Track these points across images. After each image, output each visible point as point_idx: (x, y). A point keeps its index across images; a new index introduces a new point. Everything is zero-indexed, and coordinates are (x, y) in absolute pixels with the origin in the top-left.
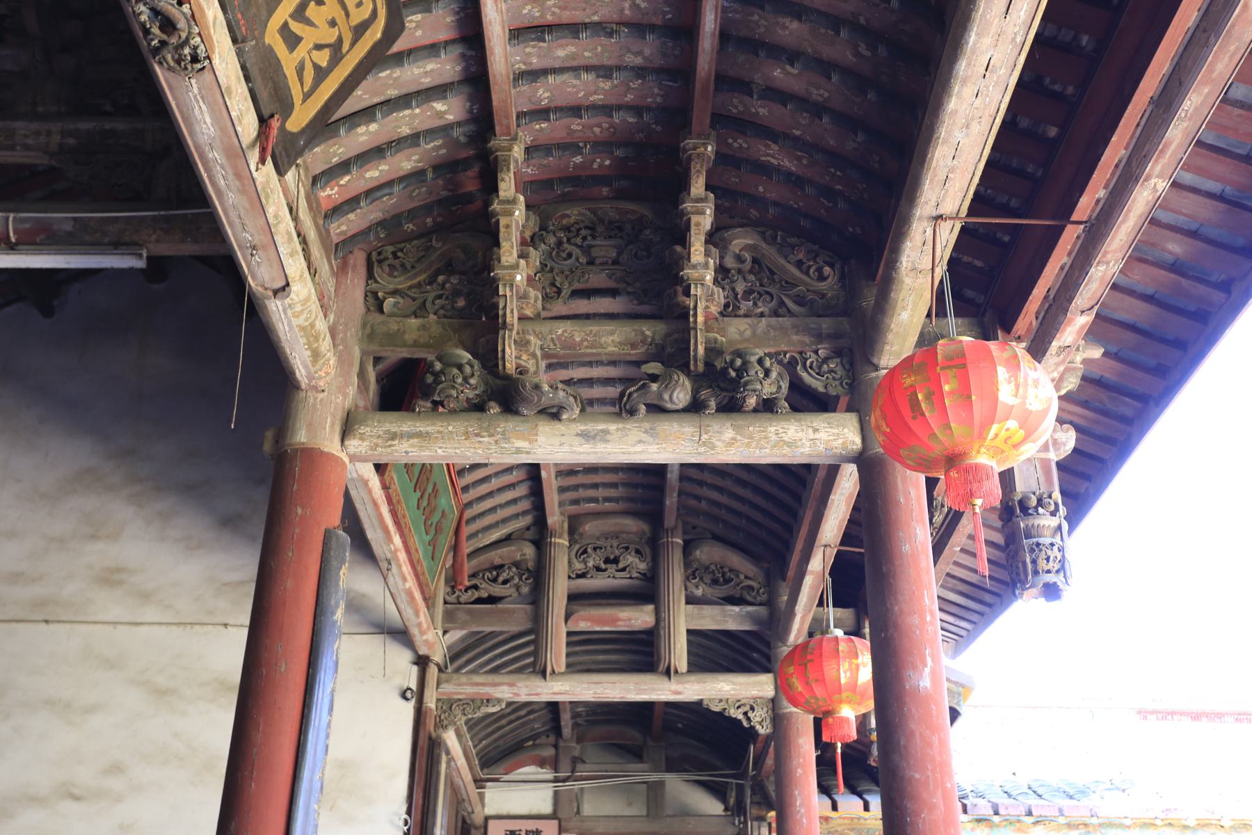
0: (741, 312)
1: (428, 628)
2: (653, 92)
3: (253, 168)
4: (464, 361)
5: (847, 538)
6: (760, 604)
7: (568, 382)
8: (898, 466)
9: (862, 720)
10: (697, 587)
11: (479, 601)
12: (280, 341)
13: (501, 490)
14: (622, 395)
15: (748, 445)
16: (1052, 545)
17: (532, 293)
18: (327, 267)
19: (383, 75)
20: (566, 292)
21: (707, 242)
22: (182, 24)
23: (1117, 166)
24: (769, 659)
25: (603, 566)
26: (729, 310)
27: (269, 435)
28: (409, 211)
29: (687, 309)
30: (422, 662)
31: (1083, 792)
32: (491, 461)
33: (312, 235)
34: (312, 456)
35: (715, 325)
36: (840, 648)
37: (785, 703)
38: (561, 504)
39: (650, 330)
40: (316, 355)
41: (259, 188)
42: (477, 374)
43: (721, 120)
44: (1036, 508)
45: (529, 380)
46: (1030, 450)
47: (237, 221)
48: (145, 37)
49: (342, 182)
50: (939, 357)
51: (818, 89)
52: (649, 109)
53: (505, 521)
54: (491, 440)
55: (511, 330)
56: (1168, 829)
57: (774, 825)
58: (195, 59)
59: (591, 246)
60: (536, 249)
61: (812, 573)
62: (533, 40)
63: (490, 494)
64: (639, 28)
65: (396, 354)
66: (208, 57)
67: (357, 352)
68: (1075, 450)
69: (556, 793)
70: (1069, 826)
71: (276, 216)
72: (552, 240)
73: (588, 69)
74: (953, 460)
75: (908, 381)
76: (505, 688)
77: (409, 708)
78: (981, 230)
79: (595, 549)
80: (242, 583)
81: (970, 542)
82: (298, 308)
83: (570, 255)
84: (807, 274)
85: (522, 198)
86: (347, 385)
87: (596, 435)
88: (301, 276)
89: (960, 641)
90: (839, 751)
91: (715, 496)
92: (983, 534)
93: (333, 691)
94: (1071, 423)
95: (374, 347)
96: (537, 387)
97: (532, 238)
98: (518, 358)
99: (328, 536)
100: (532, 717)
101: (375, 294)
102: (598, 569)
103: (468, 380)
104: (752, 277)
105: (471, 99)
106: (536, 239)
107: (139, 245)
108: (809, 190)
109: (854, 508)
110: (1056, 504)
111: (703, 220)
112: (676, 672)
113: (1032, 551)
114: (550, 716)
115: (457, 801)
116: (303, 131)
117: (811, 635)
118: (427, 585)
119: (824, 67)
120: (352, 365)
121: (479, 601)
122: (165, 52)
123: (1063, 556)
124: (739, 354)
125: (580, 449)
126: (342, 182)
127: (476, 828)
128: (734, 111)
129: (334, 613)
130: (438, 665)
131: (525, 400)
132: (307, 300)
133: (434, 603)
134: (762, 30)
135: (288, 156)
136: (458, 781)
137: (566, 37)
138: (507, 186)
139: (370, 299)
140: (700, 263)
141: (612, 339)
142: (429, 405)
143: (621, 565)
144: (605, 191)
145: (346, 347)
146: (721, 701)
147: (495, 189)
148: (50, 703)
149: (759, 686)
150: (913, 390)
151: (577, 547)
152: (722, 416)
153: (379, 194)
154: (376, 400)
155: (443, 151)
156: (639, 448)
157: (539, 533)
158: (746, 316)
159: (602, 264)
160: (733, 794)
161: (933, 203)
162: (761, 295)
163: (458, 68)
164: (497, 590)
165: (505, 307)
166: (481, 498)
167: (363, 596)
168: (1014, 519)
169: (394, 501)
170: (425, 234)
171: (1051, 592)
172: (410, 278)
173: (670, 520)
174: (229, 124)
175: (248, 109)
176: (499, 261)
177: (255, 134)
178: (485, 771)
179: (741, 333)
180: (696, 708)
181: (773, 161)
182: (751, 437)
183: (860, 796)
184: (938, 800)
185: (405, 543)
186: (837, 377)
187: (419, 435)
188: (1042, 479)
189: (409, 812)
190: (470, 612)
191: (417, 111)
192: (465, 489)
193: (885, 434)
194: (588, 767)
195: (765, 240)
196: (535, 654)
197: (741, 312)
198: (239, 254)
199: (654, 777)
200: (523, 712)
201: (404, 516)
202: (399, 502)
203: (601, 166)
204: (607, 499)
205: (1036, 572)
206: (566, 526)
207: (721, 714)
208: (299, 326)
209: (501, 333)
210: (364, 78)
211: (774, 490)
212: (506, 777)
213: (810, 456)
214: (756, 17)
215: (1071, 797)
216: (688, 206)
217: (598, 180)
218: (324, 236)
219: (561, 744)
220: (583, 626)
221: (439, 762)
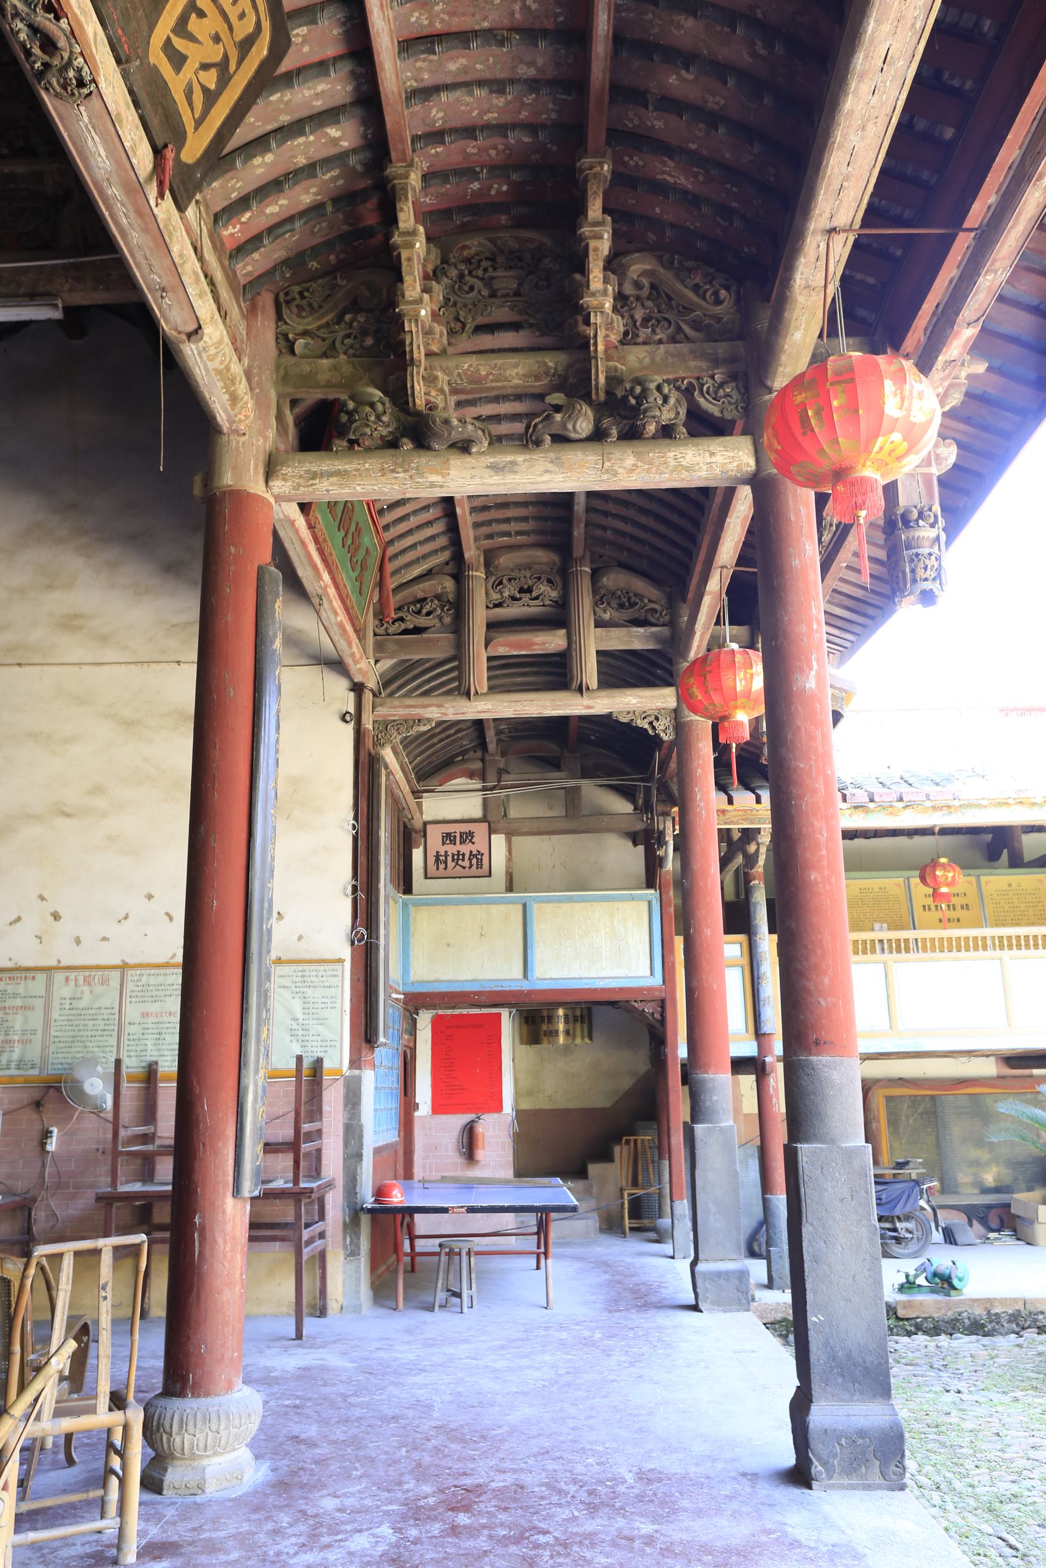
0: (640, 340)
1: (361, 658)
2: (544, 107)
3: (153, 203)
4: (376, 399)
5: (742, 559)
6: (663, 625)
7: (478, 418)
8: (789, 484)
9: (756, 722)
10: (605, 612)
11: (406, 632)
12: (198, 386)
13: (419, 527)
14: (528, 427)
15: (649, 471)
16: (930, 554)
17: (438, 328)
18: (236, 309)
19: (274, 98)
20: (469, 327)
21: (605, 269)
22: (62, 43)
23: (1010, 168)
24: (671, 674)
25: (518, 596)
26: (628, 338)
27: (198, 479)
28: (312, 248)
29: (587, 339)
30: (358, 688)
31: (948, 780)
32: (408, 496)
33: (219, 276)
34: (240, 497)
35: (616, 354)
36: (736, 660)
37: (686, 712)
38: (476, 539)
39: (553, 361)
40: (234, 398)
41: (161, 226)
42: (389, 411)
43: (620, 137)
44: (917, 521)
45: (439, 415)
46: (912, 462)
47: (144, 262)
48: (27, 59)
49: (243, 220)
50: (829, 373)
51: (714, 97)
52: (543, 126)
53: (425, 557)
54: (406, 475)
55: (418, 366)
56: (1019, 807)
57: (677, 819)
58: (81, 84)
59: (492, 278)
60: (439, 283)
61: (710, 593)
62: (423, 52)
63: (410, 532)
64: (530, 34)
65: (313, 396)
66: (94, 81)
67: (273, 395)
68: (955, 466)
69: (484, 800)
70: (934, 808)
71: (181, 256)
72: (454, 273)
73: (480, 83)
74: (840, 474)
75: (799, 399)
76: (434, 709)
77: (349, 730)
78: (875, 245)
79: (510, 580)
80: (189, 624)
81: (856, 559)
82: (212, 351)
83: (472, 288)
84: (704, 298)
85: (421, 229)
86: (266, 427)
87: (504, 467)
88: (212, 318)
89: (843, 651)
90: (734, 750)
91: (620, 525)
92: (867, 550)
93: (278, 712)
94: (954, 439)
95: (289, 389)
96: (447, 422)
97: (434, 271)
98: (427, 394)
99: (261, 571)
100: (460, 735)
101: (285, 336)
102: (514, 599)
103: (382, 420)
104: (650, 304)
105: (365, 122)
106: (439, 273)
107: (54, 295)
108: (705, 209)
109: (748, 531)
110: (936, 517)
111: (601, 245)
112: (588, 688)
113: (912, 561)
114: (476, 734)
115: (398, 809)
116: (199, 162)
117: (709, 650)
118: (357, 618)
119: (720, 70)
120: (269, 407)
121: (406, 632)
122: (49, 76)
123: (940, 565)
124: (638, 381)
125: (490, 481)
126: (243, 220)
127: (416, 832)
128: (630, 125)
129: (272, 643)
130: (372, 690)
131: (435, 435)
132: (220, 342)
133: (364, 635)
134: (656, 30)
135: (187, 191)
136: (397, 791)
137: (457, 48)
138: (406, 217)
139: (282, 342)
140: (599, 290)
141: (517, 371)
142: (345, 444)
143: (534, 594)
144: (504, 219)
145: (262, 390)
146: (628, 713)
147: (395, 221)
148: (32, 736)
149: (664, 698)
150: (803, 407)
151: (493, 578)
152: (622, 443)
153: (281, 230)
154: (296, 443)
155: (340, 182)
156: (546, 477)
157: (457, 566)
158: (644, 343)
159: (503, 296)
160: (642, 796)
161: (827, 215)
162: (659, 321)
163: (349, 88)
164: (421, 621)
165: (411, 343)
166: (401, 536)
167: (300, 631)
168: (896, 532)
169: (321, 540)
170: (329, 272)
171: (928, 598)
172: (319, 319)
173: (578, 550)
174: (124, 155)
175: (141, 139)
176: (403, 297)
177: (151, 166)
178: (421, 783)
179: (641, 361)
180: (606, 721)
181: (669, 178)
182: (651, 464)
183: (753, 792)
184: (820, 785)
185: (333, 579)
186: (733, 401)
187: (338, 473)
188: (924, 493)
189: (356, 818)
190: (398, 642)
191: (312, 138)
192: (386, 528)
193: (777, 451)
194: (512, 777)
195: (662, 264)
196: (459, 678)
197: (640, 340)
198: (149, 296)
199: (571, 783)
200: (452, 731)
201: (331, 554)
202: (325, 540)
203: (498, 191)
204: (519, 533)
205: (914, 581)
206: (482, 559)
207: (629, 726)
208: (215, 369)
209: (409, 369)
210: (254, 102)
211: (675, 518)
212: (440, 788)
213: (707, 479)
214: (650, 15)
215: (937, 784)
216: (586, 230)
217: (496, 207)
218: (231, 278)
219: (488, 758)
220: (502, 651)
221: (379, 776)
